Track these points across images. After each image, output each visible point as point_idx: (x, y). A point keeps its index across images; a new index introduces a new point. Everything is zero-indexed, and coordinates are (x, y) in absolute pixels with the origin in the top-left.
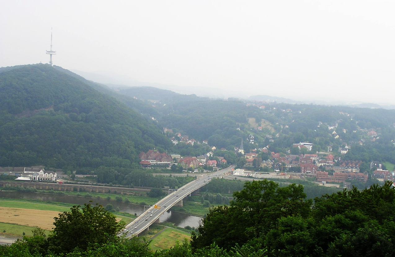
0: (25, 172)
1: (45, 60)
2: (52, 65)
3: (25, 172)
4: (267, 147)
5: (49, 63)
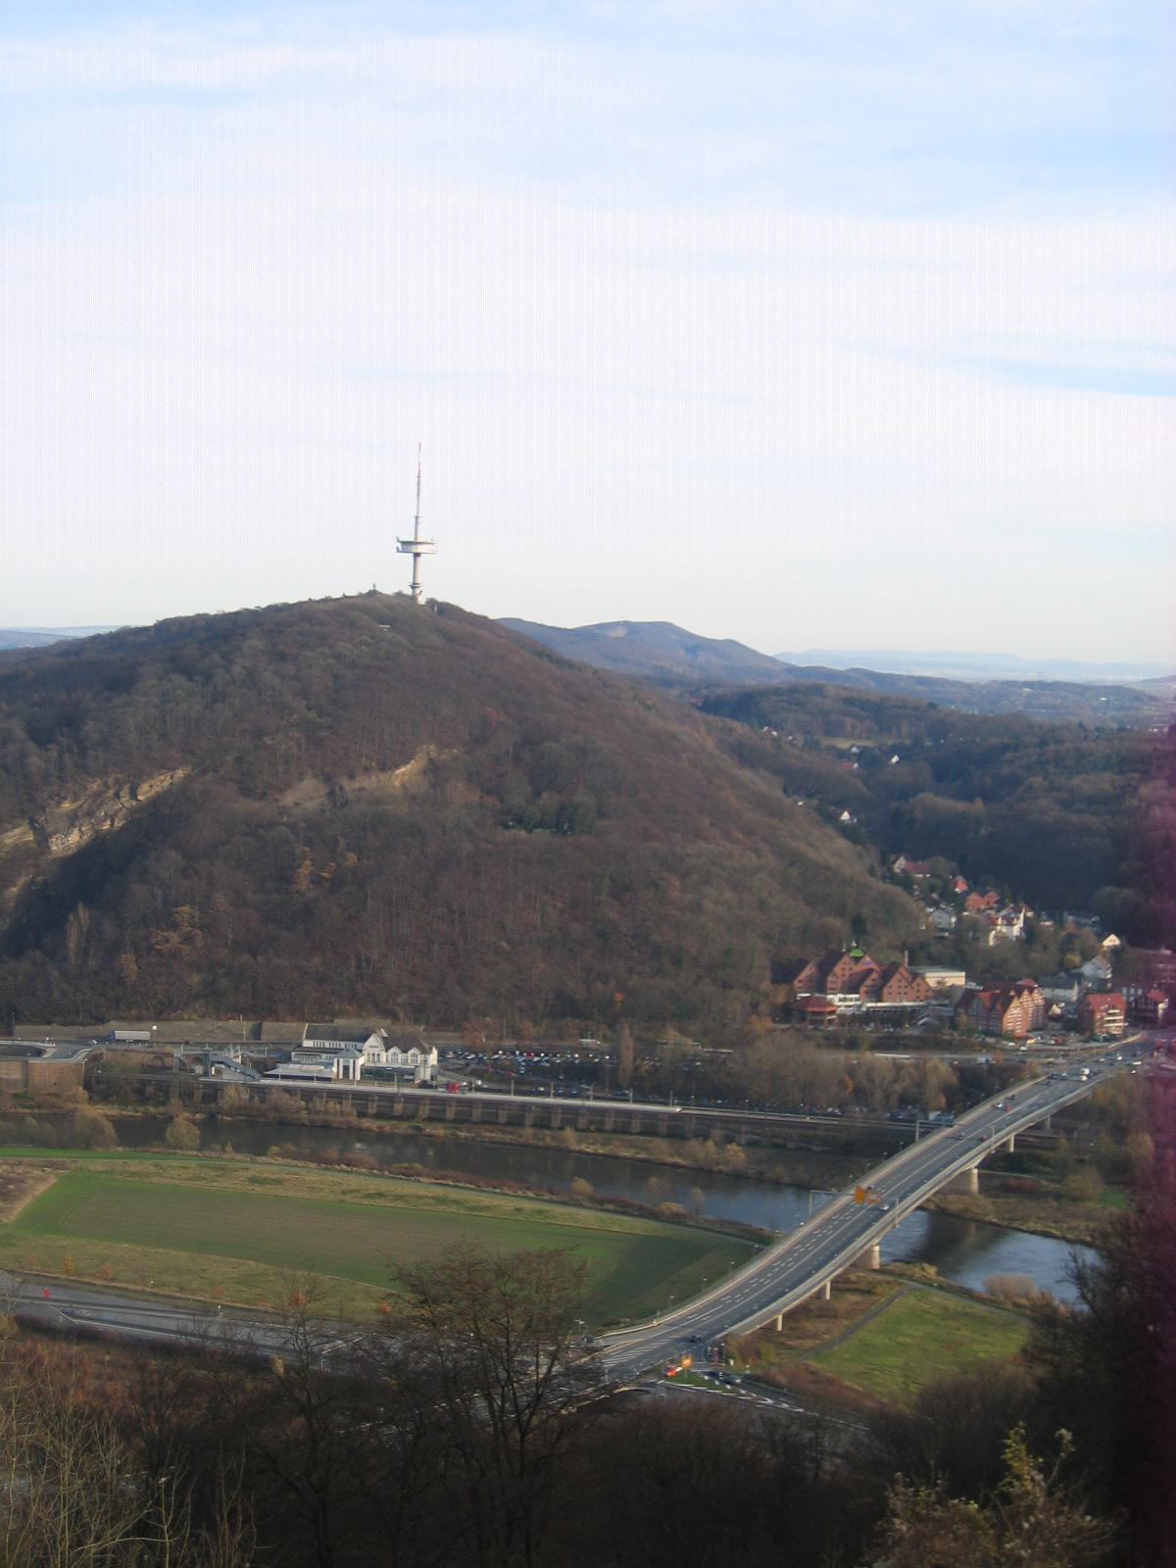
0: (308, 1043)
1: (392, 580)
2: (422, 600)
3: (308, 1043)
5: (408, 591)
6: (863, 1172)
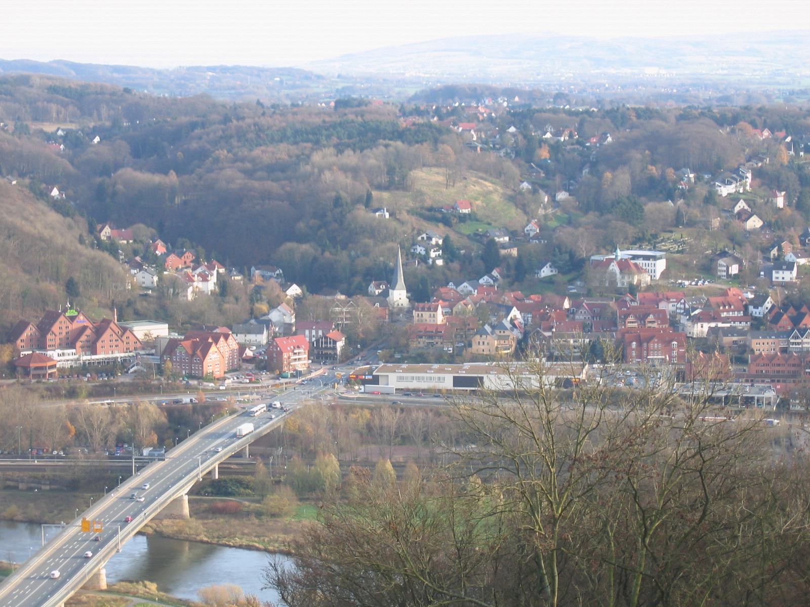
4: (495, 273)
6: (88, 505)
